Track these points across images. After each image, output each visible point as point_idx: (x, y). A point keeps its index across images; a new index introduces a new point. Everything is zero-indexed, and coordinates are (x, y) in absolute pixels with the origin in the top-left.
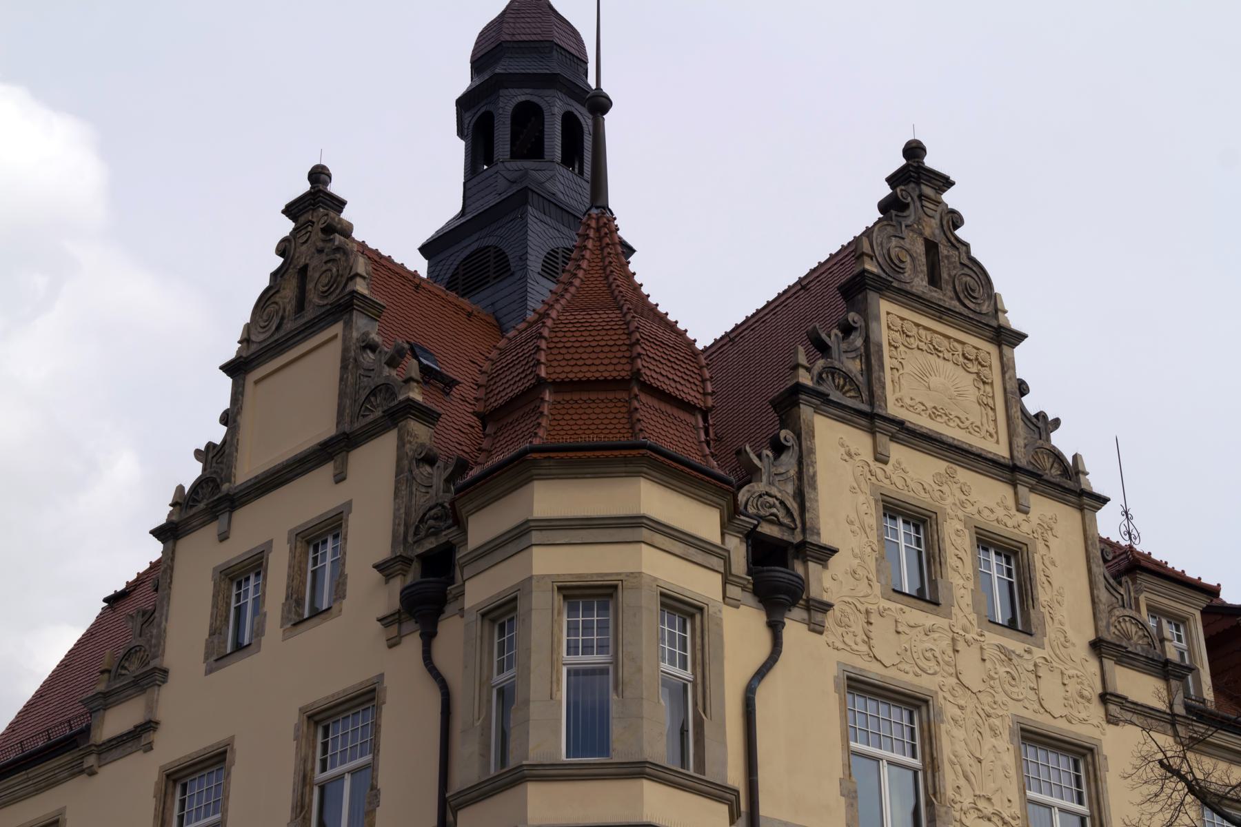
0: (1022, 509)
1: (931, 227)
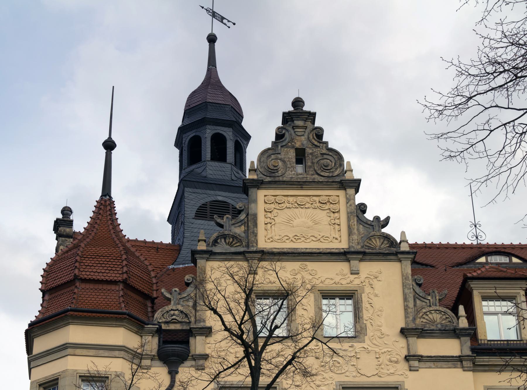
1: (301, 141)
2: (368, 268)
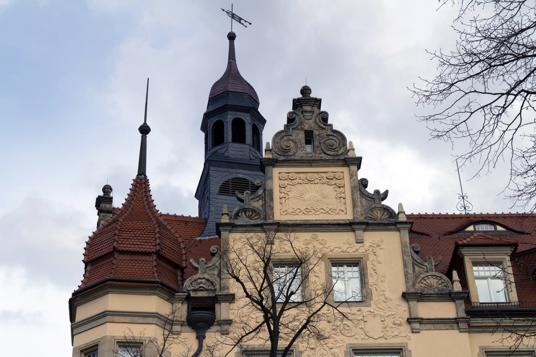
0: (360, 242)
2: (371, 238)
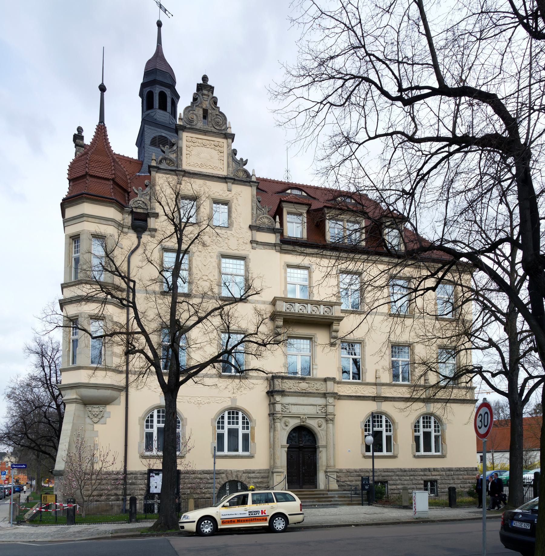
0: (230, 190)
2: (237, 188)
